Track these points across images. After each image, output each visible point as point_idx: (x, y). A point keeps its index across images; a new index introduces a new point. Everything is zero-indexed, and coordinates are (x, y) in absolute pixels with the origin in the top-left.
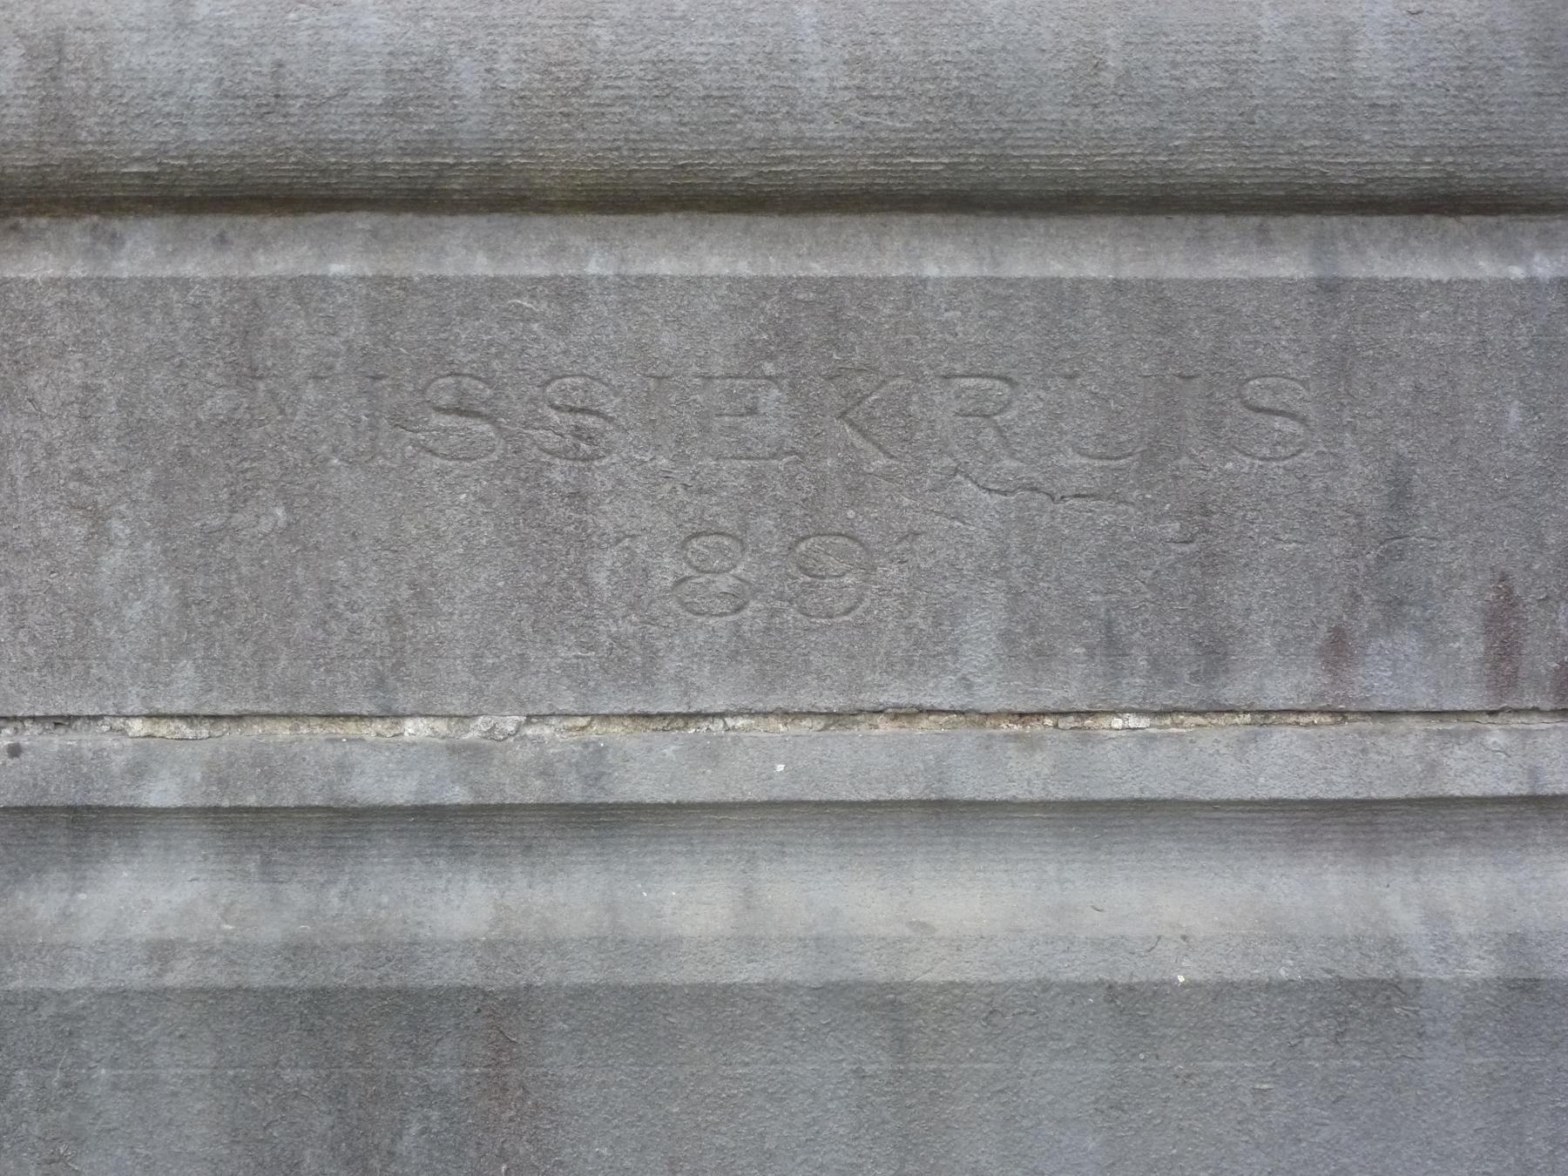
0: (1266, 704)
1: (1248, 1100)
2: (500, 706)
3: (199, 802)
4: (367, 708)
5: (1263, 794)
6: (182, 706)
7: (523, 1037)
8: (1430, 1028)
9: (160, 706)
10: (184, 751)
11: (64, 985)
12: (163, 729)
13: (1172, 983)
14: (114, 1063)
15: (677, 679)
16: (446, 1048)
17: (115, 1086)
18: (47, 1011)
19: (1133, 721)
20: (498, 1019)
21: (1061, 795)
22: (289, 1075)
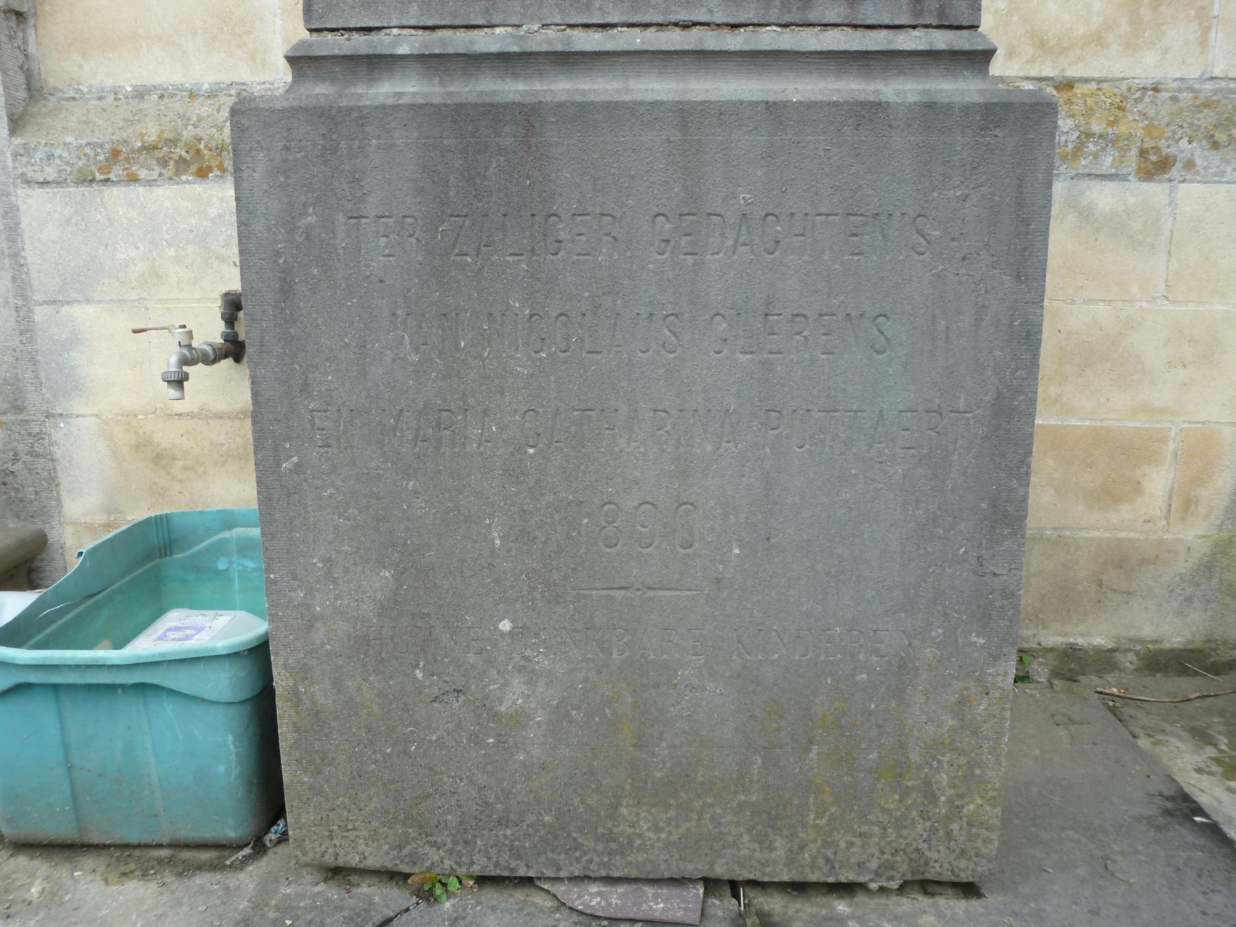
0: (825, 21)
1: (822, 154)
2: (532, 20)
3: (416, 52)
4: (481, 22)
5: (825, 49)
6: (413, 22)
7: (537, 125)
8: (894, 123)
9: (405, 23)
10: (413, 38)
11: (361, 104)
12: (405, 32)
13: (791, 102)
14: (379, 137)
15: (600, 9)
16: (508, 129)
17: (379, 148)
18: (354, 115)
19: (775, 28)
20: (529, 116)
21: (747, 48)
22: (446, 142)
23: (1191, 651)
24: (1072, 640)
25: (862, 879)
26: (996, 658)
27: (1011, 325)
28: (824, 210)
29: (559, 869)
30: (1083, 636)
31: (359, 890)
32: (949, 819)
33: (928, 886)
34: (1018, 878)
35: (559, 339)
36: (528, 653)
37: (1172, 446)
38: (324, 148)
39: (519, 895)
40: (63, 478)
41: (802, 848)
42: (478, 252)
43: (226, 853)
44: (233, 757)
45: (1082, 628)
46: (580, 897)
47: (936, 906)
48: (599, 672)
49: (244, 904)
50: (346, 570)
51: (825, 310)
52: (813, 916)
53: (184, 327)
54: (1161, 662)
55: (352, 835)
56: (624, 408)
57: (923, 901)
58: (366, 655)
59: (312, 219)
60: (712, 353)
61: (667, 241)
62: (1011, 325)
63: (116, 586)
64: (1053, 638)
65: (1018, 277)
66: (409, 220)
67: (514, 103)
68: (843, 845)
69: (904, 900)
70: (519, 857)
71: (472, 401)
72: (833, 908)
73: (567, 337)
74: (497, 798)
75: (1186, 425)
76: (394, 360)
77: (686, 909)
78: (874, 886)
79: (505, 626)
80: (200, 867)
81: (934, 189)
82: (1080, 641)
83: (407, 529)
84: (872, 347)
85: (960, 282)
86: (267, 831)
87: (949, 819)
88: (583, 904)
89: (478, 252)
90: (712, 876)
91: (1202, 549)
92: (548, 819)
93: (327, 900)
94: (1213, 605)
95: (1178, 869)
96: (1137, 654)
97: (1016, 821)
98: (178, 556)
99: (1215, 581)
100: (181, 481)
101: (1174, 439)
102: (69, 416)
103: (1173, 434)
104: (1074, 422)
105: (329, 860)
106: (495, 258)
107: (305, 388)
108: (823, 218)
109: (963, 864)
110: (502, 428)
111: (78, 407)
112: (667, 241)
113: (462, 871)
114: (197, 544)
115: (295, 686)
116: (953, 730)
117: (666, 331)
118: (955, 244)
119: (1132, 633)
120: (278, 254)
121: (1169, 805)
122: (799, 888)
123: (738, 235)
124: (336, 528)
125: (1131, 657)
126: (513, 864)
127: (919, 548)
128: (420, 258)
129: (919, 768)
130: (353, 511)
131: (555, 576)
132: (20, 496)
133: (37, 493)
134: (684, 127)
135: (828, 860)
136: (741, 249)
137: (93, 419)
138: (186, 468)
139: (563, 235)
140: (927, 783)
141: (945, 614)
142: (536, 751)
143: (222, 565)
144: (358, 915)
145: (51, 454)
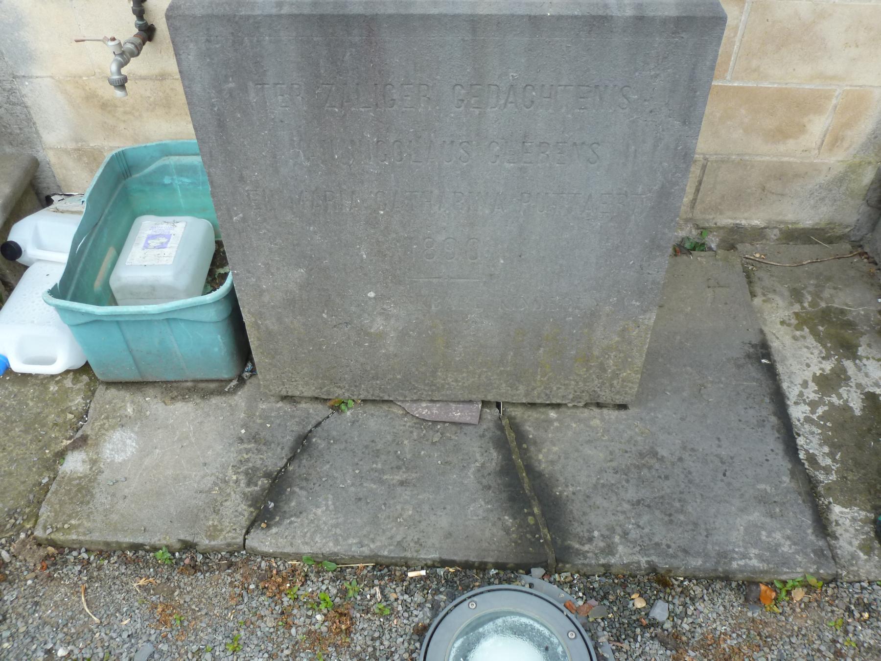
1: (565, 49)
14: (270, 36)
18: (251, 21)
22: (315, 39)
23: (817, 229)
24: (738, 222)
25: (564, 402)
26: (645, 312)
27: (676, 149)
28: (563, 83)
29: (405, 397)
30: (746, 219)
31: (301, 406)
32: (612, 379)
33: (599, 405)
34: (650, 397)
35: (396, 155)
36: (385, 306)
37: (834, 101)
38: (234, 41)
39: (385, 407)
40: (36, 118)
41: (533, 389)
42: (342, 106)
43: (224, 384)
44: (222, 344)
45: (746, 215)
46: (417, 409)
47: (602, 414)
48: (424, 315)
49: (242, 415)
50: (278, 269)
51: (560, 140)
52: (537, 419)
53: (113, 39)
54: (796, 236)
55: (295, 383)
56: (436, 192)
57: (596, 411)
58: (294, 307)
59: (232, 85)
60: (490, 163)
61: (463, 100)
62: (676, 149)
63: (106, 211)
64: (726, 220)
65: (684, 123)
66: (296, 86)
67: (359, 15)
68: (555, 388)
69: (586, 410)
70: (385, 392)
71: (345, 187)
72: (548, 415)
73: (401, 153)
74: (371, 368)
75: (848, 88)
76: (295, 165)
77: (472, 416)
78: (570, 405)
79: (372, 294)
80: (212, 393)
81: (636, 70)
82: (743, 222)
83: (312, 250)
84: (588, 160)
85: (647, 125)
86: (243, 371)
87: (612, 379)
88: (418, 413)
89: (342, 106)
90: (485, 399)
91: (841, 168)
92: (399, 377)
93: (285, 412)
94: (838, 203)
95: (738, 394)
96: (780, 230)
97: (660, 360)
98: (136, 176)
99: (843, 188)
100: (124, 121)
101: (837, 97)
102: (31, 77)
103: (837, 93)
104: (766, 85)
105: (284, 393)
106: (353, 109)
107: (242, 179)
108: (562, 88)
109: (618, 397)
110: (363, 201)
111: (35, 71)
112: (463, 100)
113: (355, 398)
114: (146, 167)
115: (256, 322)
116: (618, 342)
117: (462, 151)
118: (646, 103)
119: (780, 218)
120: (213, 105)
121: (751, 350)
122: (533, 405)
123: (508, 97)
124: (270, 249)
125: (776, 231)
126: (381, 395)
127: (606, 261)
128: (305, 108)
129: (598, 358)
130: (278, 241)
131: (398, 272)
132: (9, 131)
133: (20, 129)
134: (474, 31)
135: (546, 395)
136: (509, 105)
137: (49, 79)
138: (125, 113)
139: (395, 97)
140: (602, 364)
141: (619, 292)
142: (391, 349)
143: (167, 180)
144: (304, 421)
145: (23, 103)
